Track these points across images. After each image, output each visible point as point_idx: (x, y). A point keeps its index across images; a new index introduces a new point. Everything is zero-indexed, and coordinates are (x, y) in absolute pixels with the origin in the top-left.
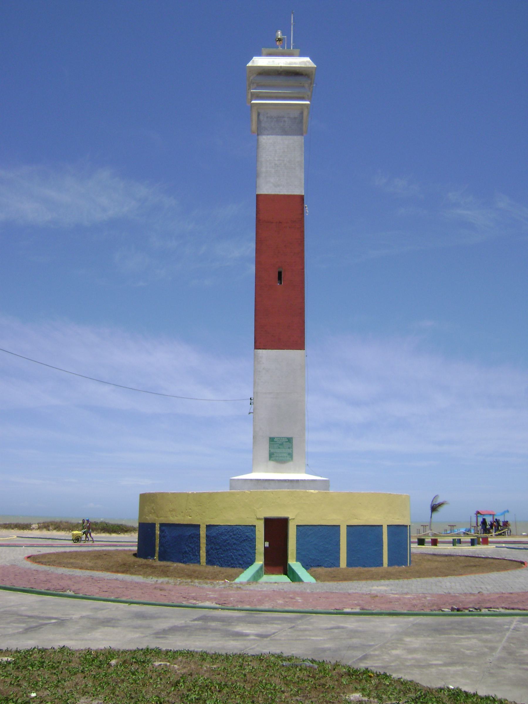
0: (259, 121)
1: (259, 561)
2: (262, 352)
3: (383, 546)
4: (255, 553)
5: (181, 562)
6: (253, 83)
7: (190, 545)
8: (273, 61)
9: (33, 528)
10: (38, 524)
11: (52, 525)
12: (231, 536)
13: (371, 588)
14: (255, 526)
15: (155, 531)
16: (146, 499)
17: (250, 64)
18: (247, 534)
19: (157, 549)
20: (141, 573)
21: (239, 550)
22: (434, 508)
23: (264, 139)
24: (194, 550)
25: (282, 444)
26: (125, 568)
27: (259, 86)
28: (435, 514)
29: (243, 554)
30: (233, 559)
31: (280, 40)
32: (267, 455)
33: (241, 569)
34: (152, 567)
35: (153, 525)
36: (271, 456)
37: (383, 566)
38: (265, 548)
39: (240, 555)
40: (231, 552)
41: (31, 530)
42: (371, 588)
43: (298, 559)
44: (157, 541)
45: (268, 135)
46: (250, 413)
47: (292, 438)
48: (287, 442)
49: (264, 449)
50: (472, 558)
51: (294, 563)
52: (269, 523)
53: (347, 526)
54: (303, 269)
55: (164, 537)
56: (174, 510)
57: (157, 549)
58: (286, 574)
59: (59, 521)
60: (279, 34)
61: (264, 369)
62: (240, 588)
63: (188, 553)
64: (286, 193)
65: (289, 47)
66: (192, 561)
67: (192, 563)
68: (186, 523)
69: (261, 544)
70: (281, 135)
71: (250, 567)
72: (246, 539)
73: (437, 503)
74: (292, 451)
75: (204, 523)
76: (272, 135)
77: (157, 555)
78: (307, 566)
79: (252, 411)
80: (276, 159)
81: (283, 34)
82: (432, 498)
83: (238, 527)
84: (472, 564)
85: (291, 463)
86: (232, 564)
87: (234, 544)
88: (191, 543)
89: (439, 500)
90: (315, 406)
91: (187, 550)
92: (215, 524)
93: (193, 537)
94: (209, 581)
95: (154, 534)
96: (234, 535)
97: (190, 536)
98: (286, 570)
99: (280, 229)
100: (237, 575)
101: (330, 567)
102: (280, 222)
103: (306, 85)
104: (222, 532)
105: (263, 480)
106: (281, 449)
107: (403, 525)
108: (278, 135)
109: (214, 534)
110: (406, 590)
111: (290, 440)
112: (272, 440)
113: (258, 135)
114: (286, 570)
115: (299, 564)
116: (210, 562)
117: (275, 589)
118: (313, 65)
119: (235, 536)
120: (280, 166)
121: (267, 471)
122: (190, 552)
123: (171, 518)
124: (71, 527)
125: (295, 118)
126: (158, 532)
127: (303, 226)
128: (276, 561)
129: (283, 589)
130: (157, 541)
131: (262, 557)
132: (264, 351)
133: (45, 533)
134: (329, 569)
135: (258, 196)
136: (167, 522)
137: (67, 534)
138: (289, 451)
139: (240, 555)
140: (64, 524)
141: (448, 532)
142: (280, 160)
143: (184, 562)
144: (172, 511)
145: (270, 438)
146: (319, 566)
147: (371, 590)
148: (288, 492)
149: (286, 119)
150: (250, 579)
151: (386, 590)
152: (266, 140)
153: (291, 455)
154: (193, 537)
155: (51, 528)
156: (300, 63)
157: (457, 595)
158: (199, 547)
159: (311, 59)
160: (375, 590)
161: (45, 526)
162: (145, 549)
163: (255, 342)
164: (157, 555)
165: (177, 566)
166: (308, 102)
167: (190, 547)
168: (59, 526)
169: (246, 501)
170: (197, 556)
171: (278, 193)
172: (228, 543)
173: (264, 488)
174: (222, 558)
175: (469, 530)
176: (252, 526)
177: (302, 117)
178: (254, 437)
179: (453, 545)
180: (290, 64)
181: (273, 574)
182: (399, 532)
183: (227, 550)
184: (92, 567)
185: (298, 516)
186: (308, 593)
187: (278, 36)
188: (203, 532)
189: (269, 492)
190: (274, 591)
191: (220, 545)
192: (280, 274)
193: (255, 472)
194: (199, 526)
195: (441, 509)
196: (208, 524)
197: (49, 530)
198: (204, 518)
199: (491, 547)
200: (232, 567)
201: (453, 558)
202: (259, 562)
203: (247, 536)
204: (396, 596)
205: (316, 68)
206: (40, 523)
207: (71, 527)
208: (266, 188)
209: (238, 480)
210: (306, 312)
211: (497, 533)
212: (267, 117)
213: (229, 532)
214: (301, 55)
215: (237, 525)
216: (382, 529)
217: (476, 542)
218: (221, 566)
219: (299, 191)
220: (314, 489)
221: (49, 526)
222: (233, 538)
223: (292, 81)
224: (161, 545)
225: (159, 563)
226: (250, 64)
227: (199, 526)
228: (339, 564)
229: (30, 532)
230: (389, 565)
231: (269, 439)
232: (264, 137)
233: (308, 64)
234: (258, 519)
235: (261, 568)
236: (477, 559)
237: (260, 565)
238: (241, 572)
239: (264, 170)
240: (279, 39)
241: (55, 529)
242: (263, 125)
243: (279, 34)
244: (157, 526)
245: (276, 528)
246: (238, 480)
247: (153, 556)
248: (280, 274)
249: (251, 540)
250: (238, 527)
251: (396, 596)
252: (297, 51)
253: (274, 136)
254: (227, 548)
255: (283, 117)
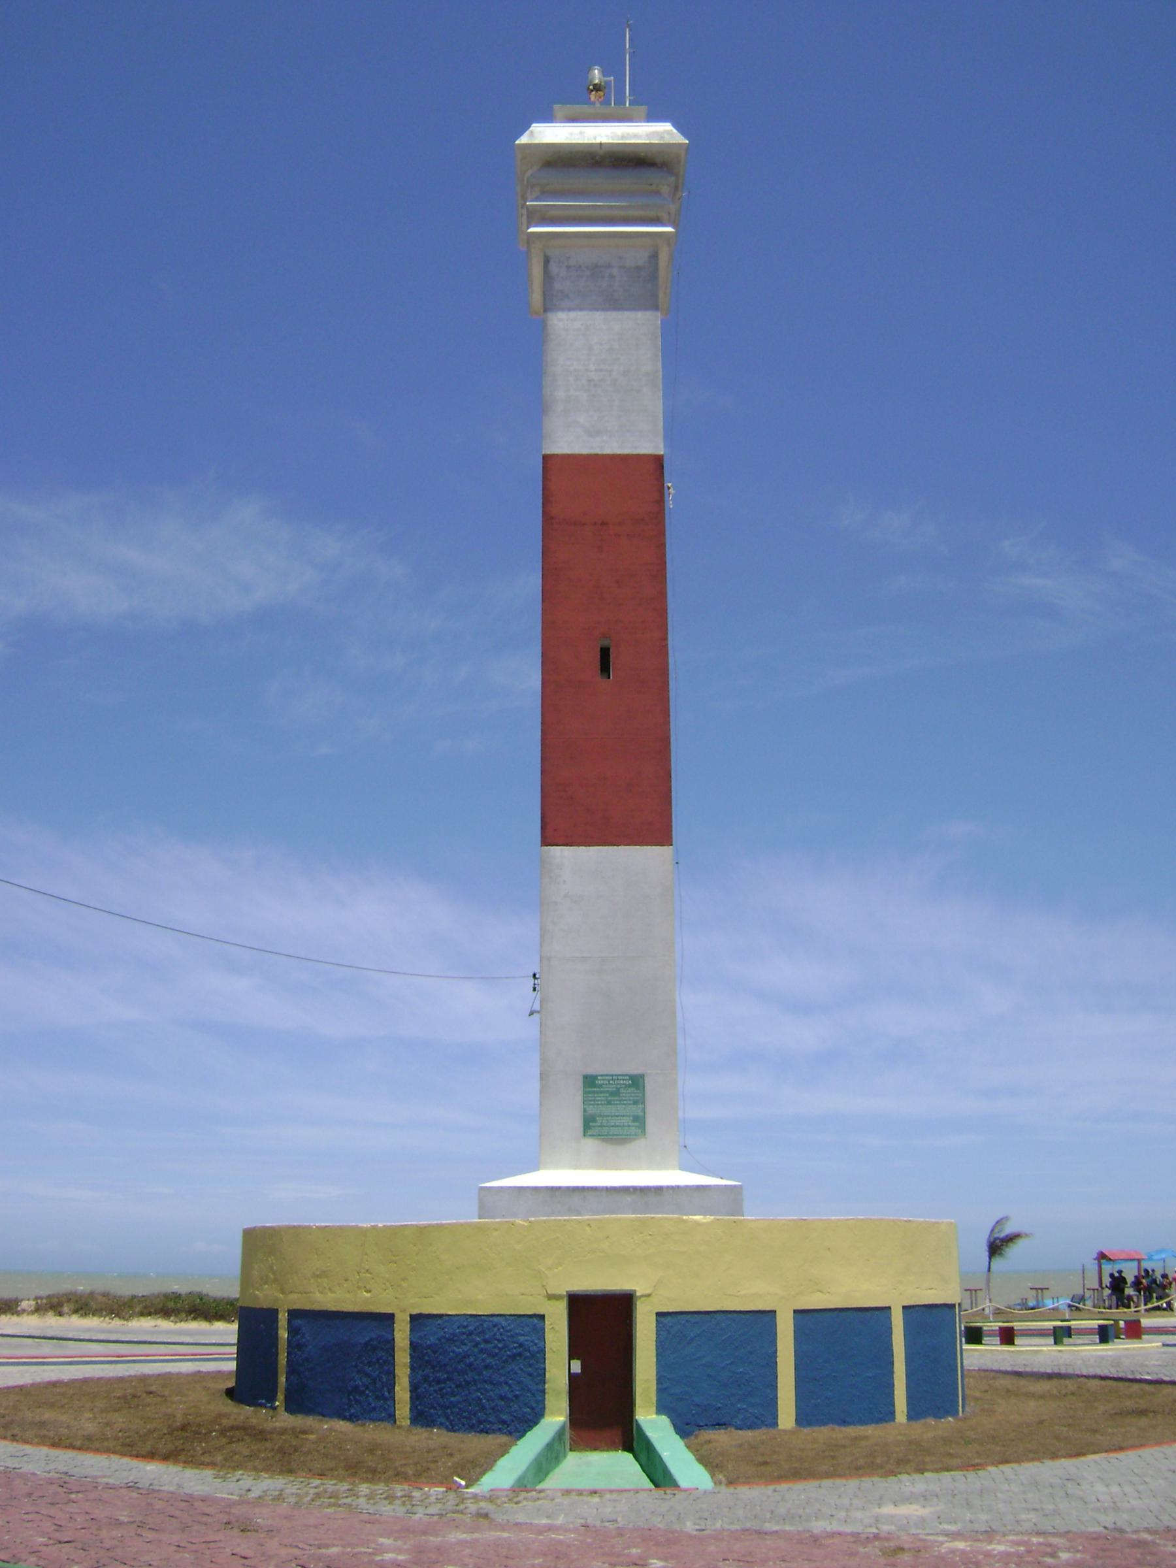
0: (548, 277)
1: (553, 1414)
2: (556, 851)
3: (892, 1363)
4: (543, 1392)
5: (344, 1418)
6: (533, 186)
7: (368, 1369)
8: (581, 133)
9: (24, 1311)
10: (36, 1298)
11: (69, 1300)
12: (476, 1345)
13: (877, 1510)
14: (542, 1317)
15: (277, 1329)
16: (258, 1242)
17: (524, 140)
18: (522, 1339)
19: (282, 1379)
20: (219, 1458)
21: (499, 1384)
22: (996, 1247)
23: (560, 320)
24: (379, 1384)
25: (617, 1093)
26: (181, 1441)
27: (545, 193)
28: (997, 1263)
29: (510, 1395)
30: (483, 1408)
31: (597, 88)
32: (578, 1123)
33: (504, 1439)
34: (261, 1435)
35: (273, 1313)
36: (589, 1125)
37: (893, 1419)
38: (572, 1377)
39: (502, 1398)
40: (478, 1390)
41: (18, 1313)
42: (877, 1510)
43: (661, 1409)
44: (283, 1359)
45: (570, 310)
46: (531, 1013)
47: (642, 1076)
48: (629, 1086)
49: (570, 1107)
50: (1121, 1384)
51: (653, 1423)
52: (583, 1308)
53: (795, 1311)
54: (665, 639)
55: (300, 1346)
56: (323, 1274)
57: (282, 1379)
58: (628, 1448)
59: (88, 1291)
60: (596, 75)
61: (566, 896)
62: (486, 1516)
63: (363, 1393)
64: (618, 451)
65: (620, 101)
66: (374, 1415)
67: (373, 1420)
68: (356, 1310)
69: (559, 1367)
70: (604, 309)
71: (528, 1434)
72: (520, 1354)
73: (1002, 1235)
74: (644, 1111)
75: (404, 1311)
76: (581, 309)
77: (281, 1396)
78: (684, 1428)
79: (537, 1007)
80: (592, 367)
81: (604, 73)
82: (993, 1223)
83: (495, 1319)
84: (1129, 1404)
85: (641, 1142)
86: (480, 1422)
87: (487, 1367)
88: (370, 1364)
89: (1008, 1229)
90: (699, 1012)
91: (358, 1382)
92: (435, 1312)
93: (374, 1348)
94: (399, 1489)
95: (275, 1338)
96: (486, 1341)
97: (366, 1344)
98: (629, 1438)
99: (604, 551)
100: (485, 1463)
101: (750, 1427)
102: (603, 524)
103: (665, 190)
104: (454, 1334)
105: (568, 1188)
106: (613, 1106)
107: (945, 1305)
108: (597, 310)
109: (432, 1340)
110: (983, 1519)
111: (637, 1081)
112: (589, 1081)
113: (545, 310)
114: (629, 1438)
115: (664, 1420)
116: (420, 1417)
117: (590, 1521)
118: (680, 139)
119: (490, 1346)
120: (602, 385)
121: (577, 1166)
122: (367, 1388)
123: (318, 1295)
124: (116, 1307)
125: (638, 268)
126: (283, 1334)
127: (662, 533)
128: (603, 1414)
129: (615, 1521)
130: (283, 1359)
131: (564, 1404)
132: (567, 850)
133: (52, 1323)
134: (748, 1435)
135: (546, 458)
136: (308, 1307)
137: (104, 1325)
138: (636, 1110)
139: (502, 1398)
140: (100, 1298)
141: (1031, 1304)
142: (601, 370)
143: (351, 1418)
144: (318, 1276)
145: (586, 1077)
146: (720, 1424)
147: (877, 1519)
148: (632, 1220)
149: (615, 271)
150: (526, 1472)
151: (922, 1521)
152: (567, 324)
153: (640, 1122)
154: (374, 1348)
155: (66, 1309)
156: (648, 135)
157: (1146, 1536)
158: (391, 1374)
159: (674, 125)
160: (891, 1518)
161: (53, 1305)
162: (252, 1382)
163: (543, 828)
164: (281, 1396)
165: (330, 1430)
166: (669, 229)
167: (368, 1375)
168: (87, 1305)
169: (518, 1247)
170: (386, 1399)
171: (598, 451)
172: (471, 1365)
173: (570, 1211)
174: (452, 1405)
175: (1082, 1299)
176: (535, 1316)
177: (656, 269)
178: (543, 1076)
179: (1056, 1343)
180: (623, 137)
181: (595, 1449)
182: (929, 1320)
183: (468, 1383)
184: (89, 1438)
185: (660, 1287)
186: (690, 1537)
187: (594, 78)
188: (402, 1335)
189: (579, 1222)
190: (586, 1526)
191: (449, 1369)
192: (605, 653)
193: (545, 1168)
194: (390, 1317)
195: (1014, 1251)
196: (415, 1312)
197: (61, 1314)
198: (404, 1296)
199: (1150, 1345)
200: (482, 1431)
201: (1070, 1385)
202: (556, 1417)
203: (521, 1345)
204: (960, 1545)
205: (688, 148)
206: (41, 1298)
207: (116, 1307)
208: (568, 438)
209: (501, 1189)
210: (673, 793)
211: (1150, 1306)
212: (568, 267)
213: (471, 1334)
214: (651, 117)
215: (492, 1315)
216: (889, 1317)
217: (1111, 1333)
218: (452, 1428)
219: (649, 444)
220: (704, 1213)
221: (60, 1305)
222: (481, 1351)
223: (628, 179)
224: (292, 1370)
225: (285, 1420)
226: (524, 140)
227: (390, 1317)
228: (775, 1416)
229: (15, 1319)
230: (910, 1417)
231: (581, 1079)
232: (562, 315)
233: (667, 136)
234: (551, 1297)
235: (560, 1434)
236: (1136, 1386)
237: (556, 1428)
238: (504, 1450)
239: (560, 394)
240: (595, 85)
241: (76, 1311)
242: (557, 286)
243: (596, 75)
244: (283, 1318)
245: (601, 1321)
246: (501, 1189)
247: (273, 1398)
248: (605, 653)
249: (533, 1356)
250: (495, 1319)
251: (960, 1545)
252: (643, 109)
253: (584, 313)
254: (468, 1379)
255: (609, 266)
